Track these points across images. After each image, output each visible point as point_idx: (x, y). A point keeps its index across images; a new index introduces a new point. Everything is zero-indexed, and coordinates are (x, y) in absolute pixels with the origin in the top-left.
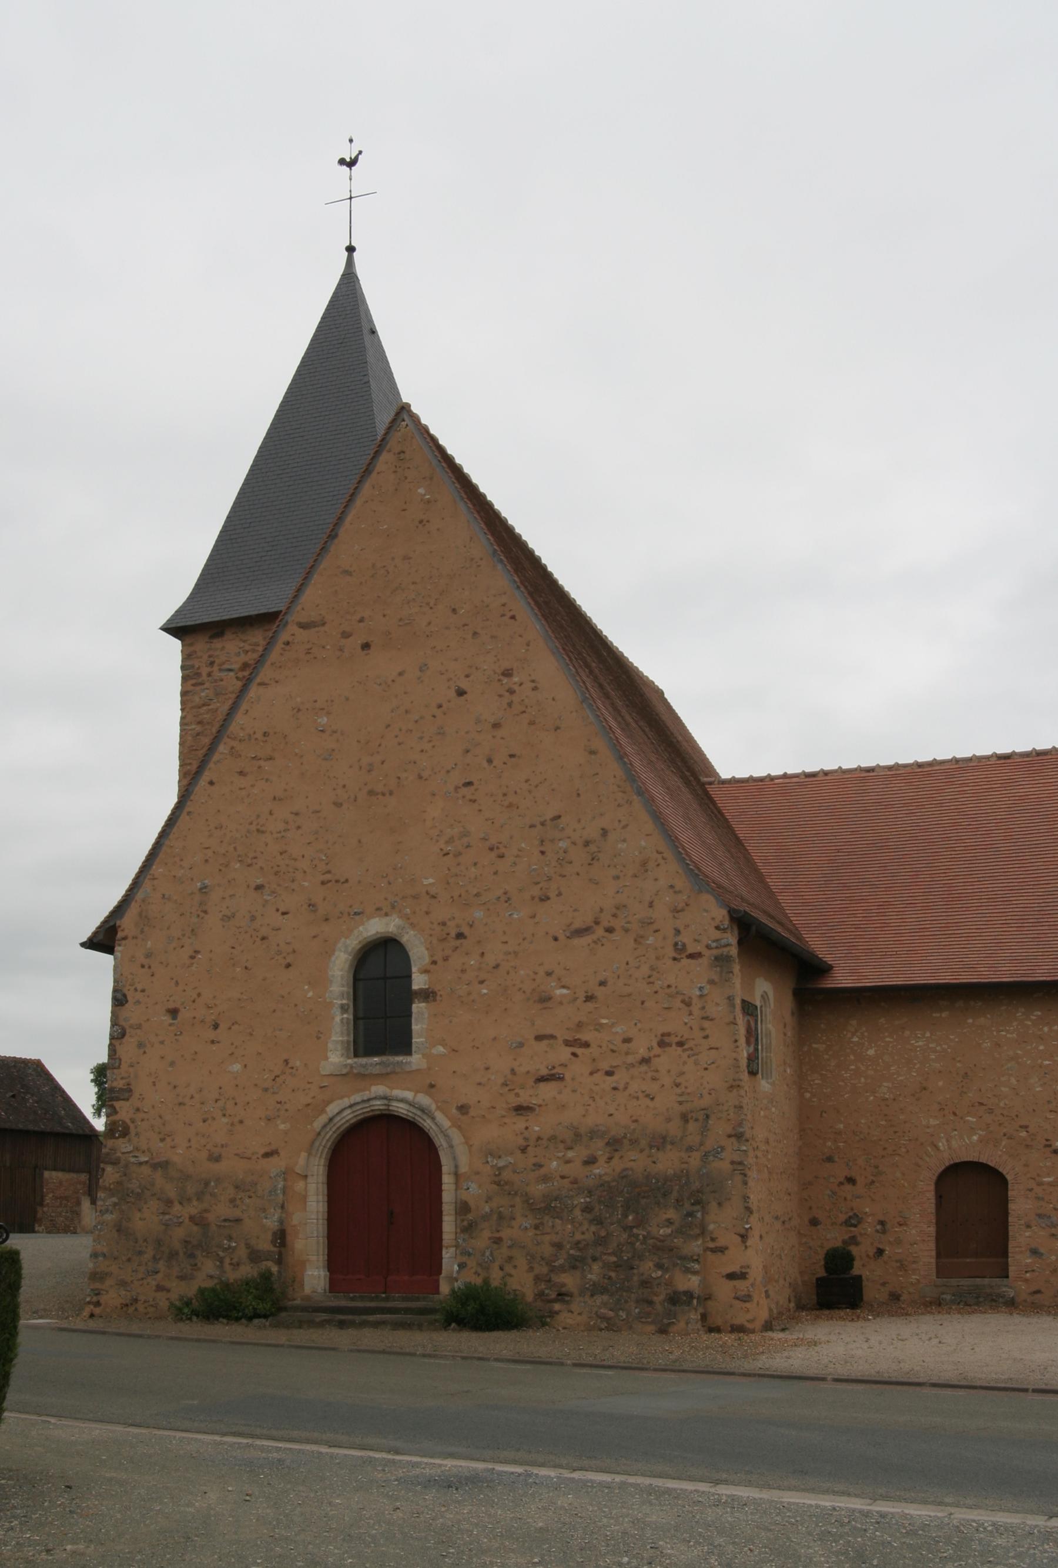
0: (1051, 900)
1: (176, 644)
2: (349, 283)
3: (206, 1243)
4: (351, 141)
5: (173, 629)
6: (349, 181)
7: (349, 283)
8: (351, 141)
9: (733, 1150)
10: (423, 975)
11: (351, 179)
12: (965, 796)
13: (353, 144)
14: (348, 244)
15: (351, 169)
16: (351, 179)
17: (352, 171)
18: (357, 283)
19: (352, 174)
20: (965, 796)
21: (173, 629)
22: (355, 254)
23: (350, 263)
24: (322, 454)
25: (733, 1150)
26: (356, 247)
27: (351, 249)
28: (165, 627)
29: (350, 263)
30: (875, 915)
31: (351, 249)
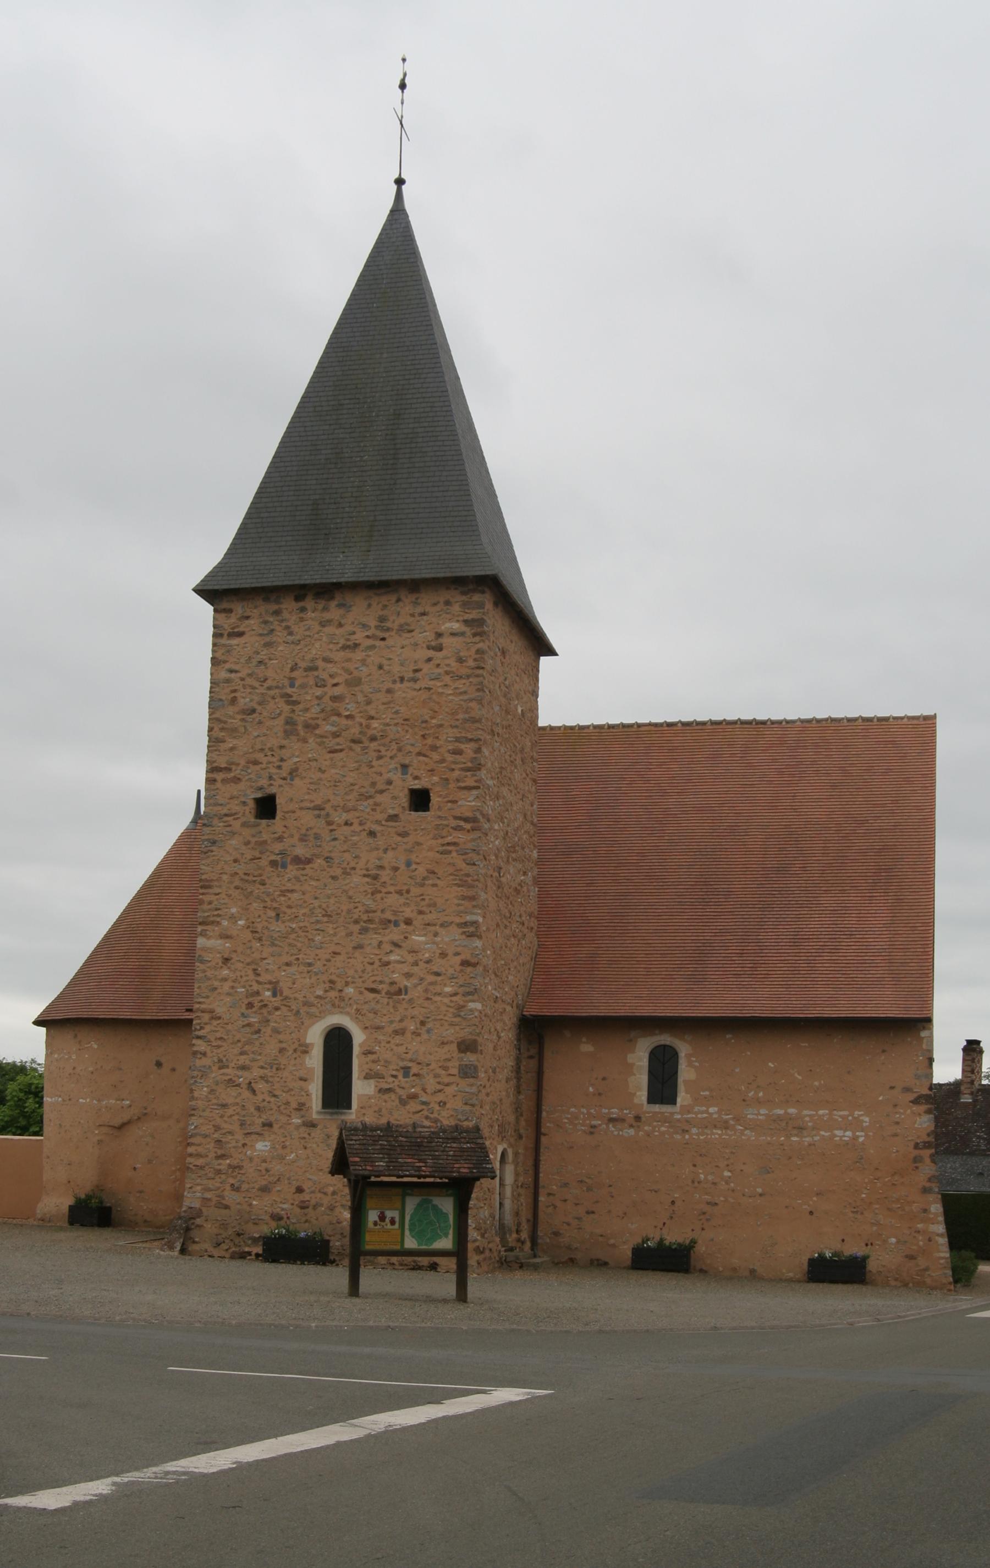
0: (851, 993)
1: (206, 610)
2: (398, 215)
3: (854, 1208)
4: (404, 60)
5: (207, 591)
6: (401, 105)
7: (398, 215)
8: (404, 60)
9: (245, 733)
10: (659, 1239)
11: (402, 103)
12: (828, 832)
13: (406, 63)
14: (397, 176)
15: (403, 92)
16: (402, 103)
17: (405, 94)
18: (435, 328)
19: (404, 98)
20: (828, 832)
21: (207, 591)
22: (403, 187)
23: (399, 197)
24: (352, 380)
25: (245, 733)
26: (407, 181)
27: (400, 182)
28: (200, 588)
29: (399, 197)
30: (824, 750)
31: (400, 182)
